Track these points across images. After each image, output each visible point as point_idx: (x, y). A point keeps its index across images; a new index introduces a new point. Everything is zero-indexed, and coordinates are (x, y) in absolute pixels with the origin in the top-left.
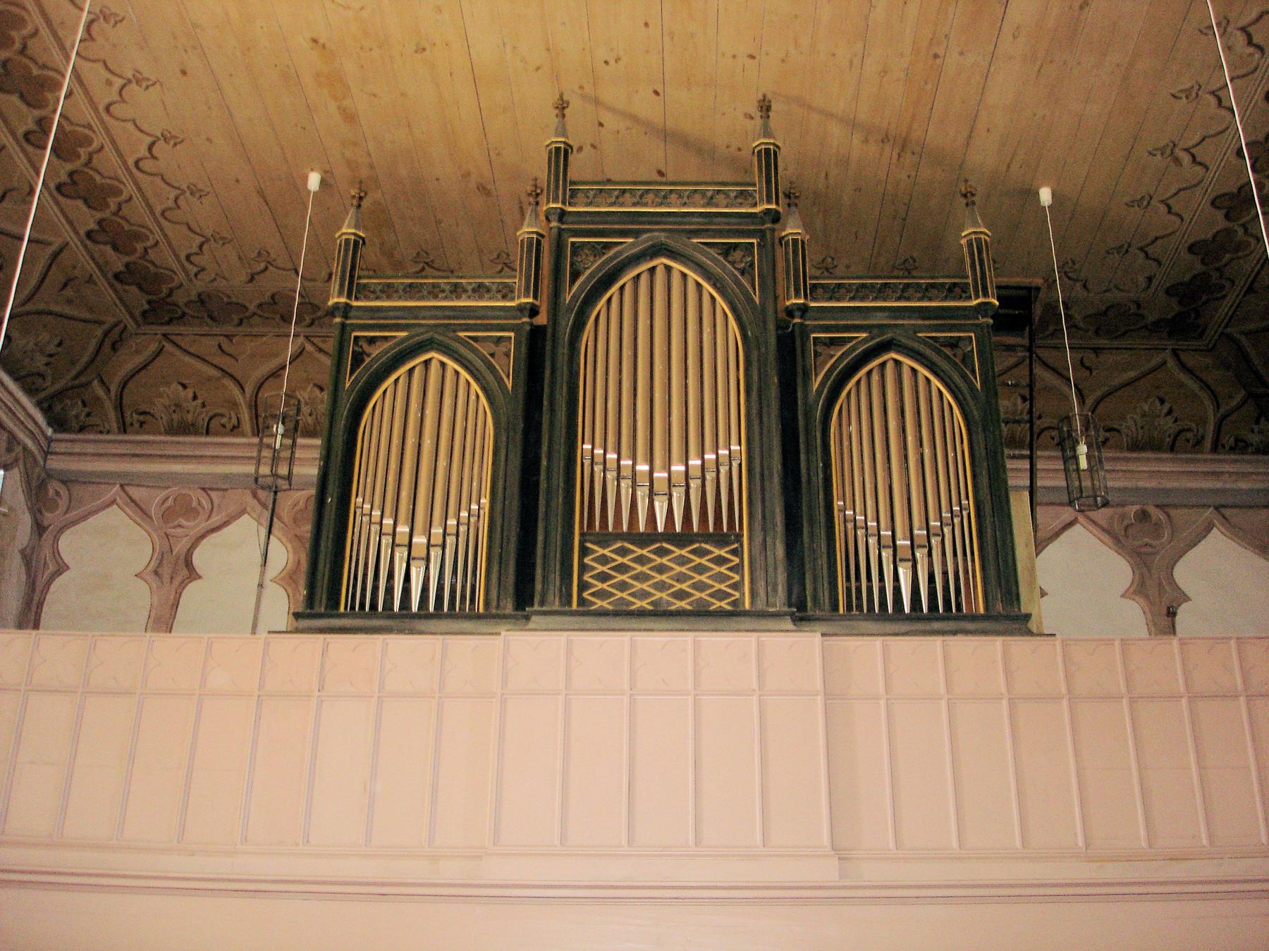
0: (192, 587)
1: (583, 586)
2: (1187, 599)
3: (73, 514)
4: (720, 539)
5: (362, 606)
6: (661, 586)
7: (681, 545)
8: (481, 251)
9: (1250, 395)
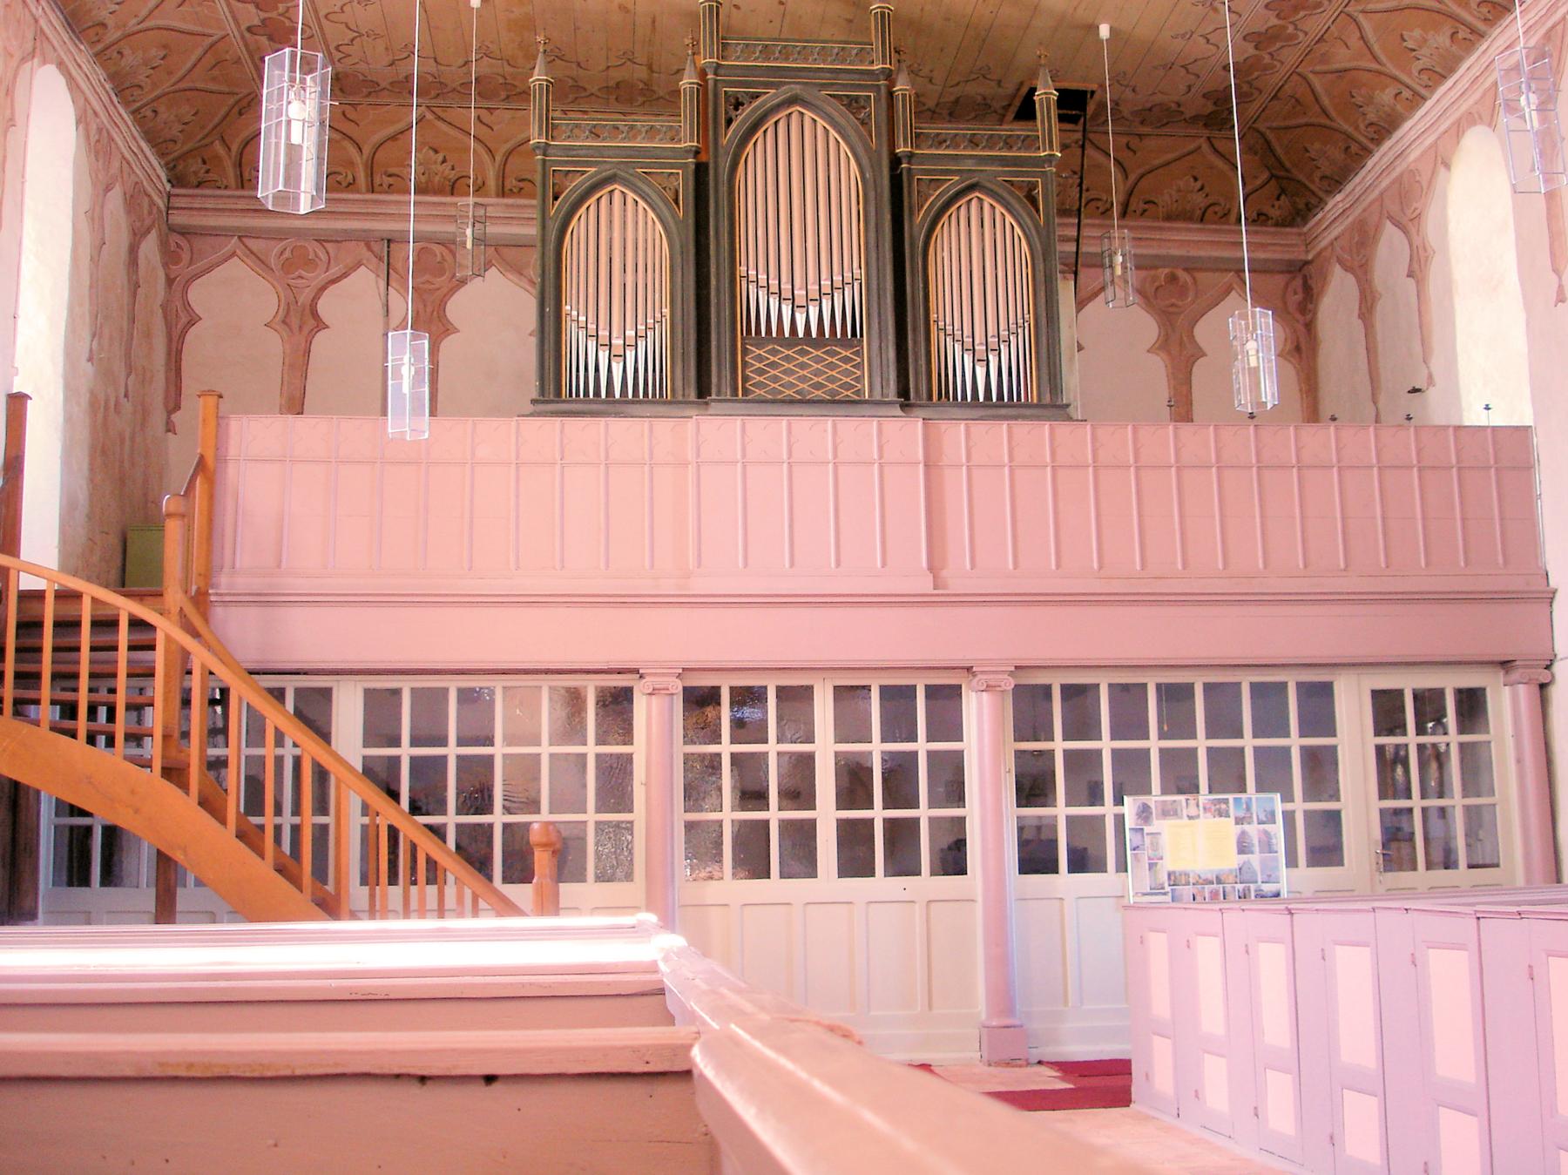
0: (321, 337)
1: (745, 379)
2: (1204, 355)
3: (200, 265)
4: (844, 342)
5: (586, 393)
6: (803, 379)
7: (817, 347)
8: (609, 49)
9: (1272, 176)
